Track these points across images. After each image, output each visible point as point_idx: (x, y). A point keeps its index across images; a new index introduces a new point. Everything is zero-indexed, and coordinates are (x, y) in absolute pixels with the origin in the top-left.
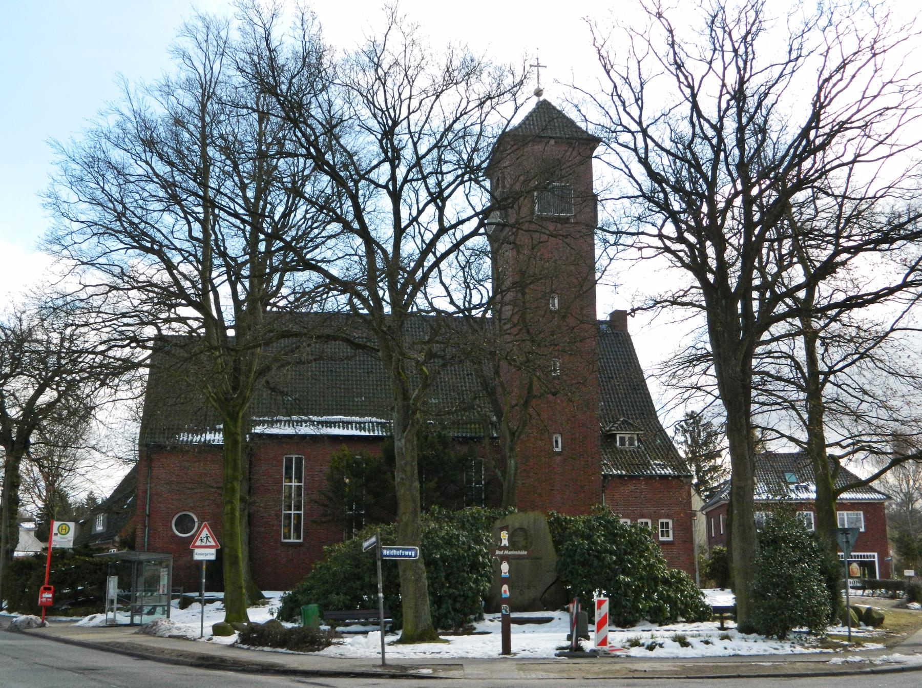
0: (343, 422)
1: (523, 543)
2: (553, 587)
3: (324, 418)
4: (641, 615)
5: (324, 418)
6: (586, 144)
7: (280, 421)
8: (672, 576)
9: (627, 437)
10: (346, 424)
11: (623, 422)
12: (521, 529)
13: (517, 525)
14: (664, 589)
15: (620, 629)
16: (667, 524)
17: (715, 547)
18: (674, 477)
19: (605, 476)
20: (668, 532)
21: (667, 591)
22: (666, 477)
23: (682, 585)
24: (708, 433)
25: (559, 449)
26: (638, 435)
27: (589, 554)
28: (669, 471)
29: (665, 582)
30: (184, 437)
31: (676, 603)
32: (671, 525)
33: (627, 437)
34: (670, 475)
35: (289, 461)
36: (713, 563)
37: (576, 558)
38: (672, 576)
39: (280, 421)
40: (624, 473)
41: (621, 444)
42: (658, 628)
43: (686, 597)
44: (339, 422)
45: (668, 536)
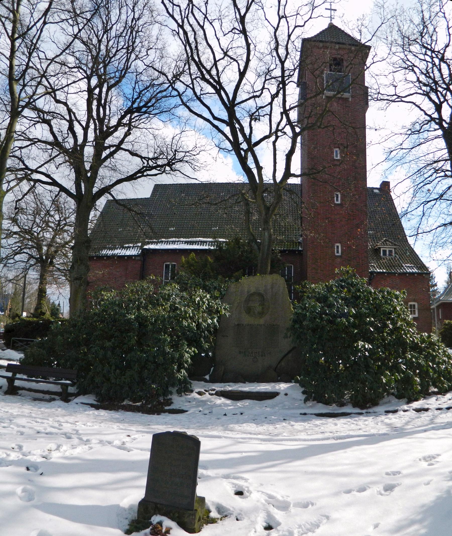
0: (201, 242)
1: (259, 309)
2: (290, 355)
3: (190, 239)
4: (385, 390)
5: (190, 239)
6: (363, 50)
7: (162, 242)
8: (423, 341)
9: (387, 250)
10: (202, 243)
11: (385, 241)
12: (260, 295)
13: (253, 290)
14: (413, 356)
15: (358, 410)
16: (414, 305)
17: (445, 321)
18: (418, 274)
19: (372, 273)
20: (414, 311)
21: (416, 358)
22: (413, 274)
23: (434, 351)
24: (311, 529)
25: (340, 254)
26: (395, 248)
27: (322, 319)
28: (415, 270)
29: (415, 347)
30: (104, 252)
31: (427, 372)
32: (416, 307)
33: (387, 250)
34: (416, 273)
35: (167, 266)
36: (444, 331)
37: (305, 323)
38: (423, 341)
39: (162, 242)
40: (384, 271)
41: (383, 255)
42: (405, 407)
43: (438, 364)
44: (198, 242)
45: (415, 314)
